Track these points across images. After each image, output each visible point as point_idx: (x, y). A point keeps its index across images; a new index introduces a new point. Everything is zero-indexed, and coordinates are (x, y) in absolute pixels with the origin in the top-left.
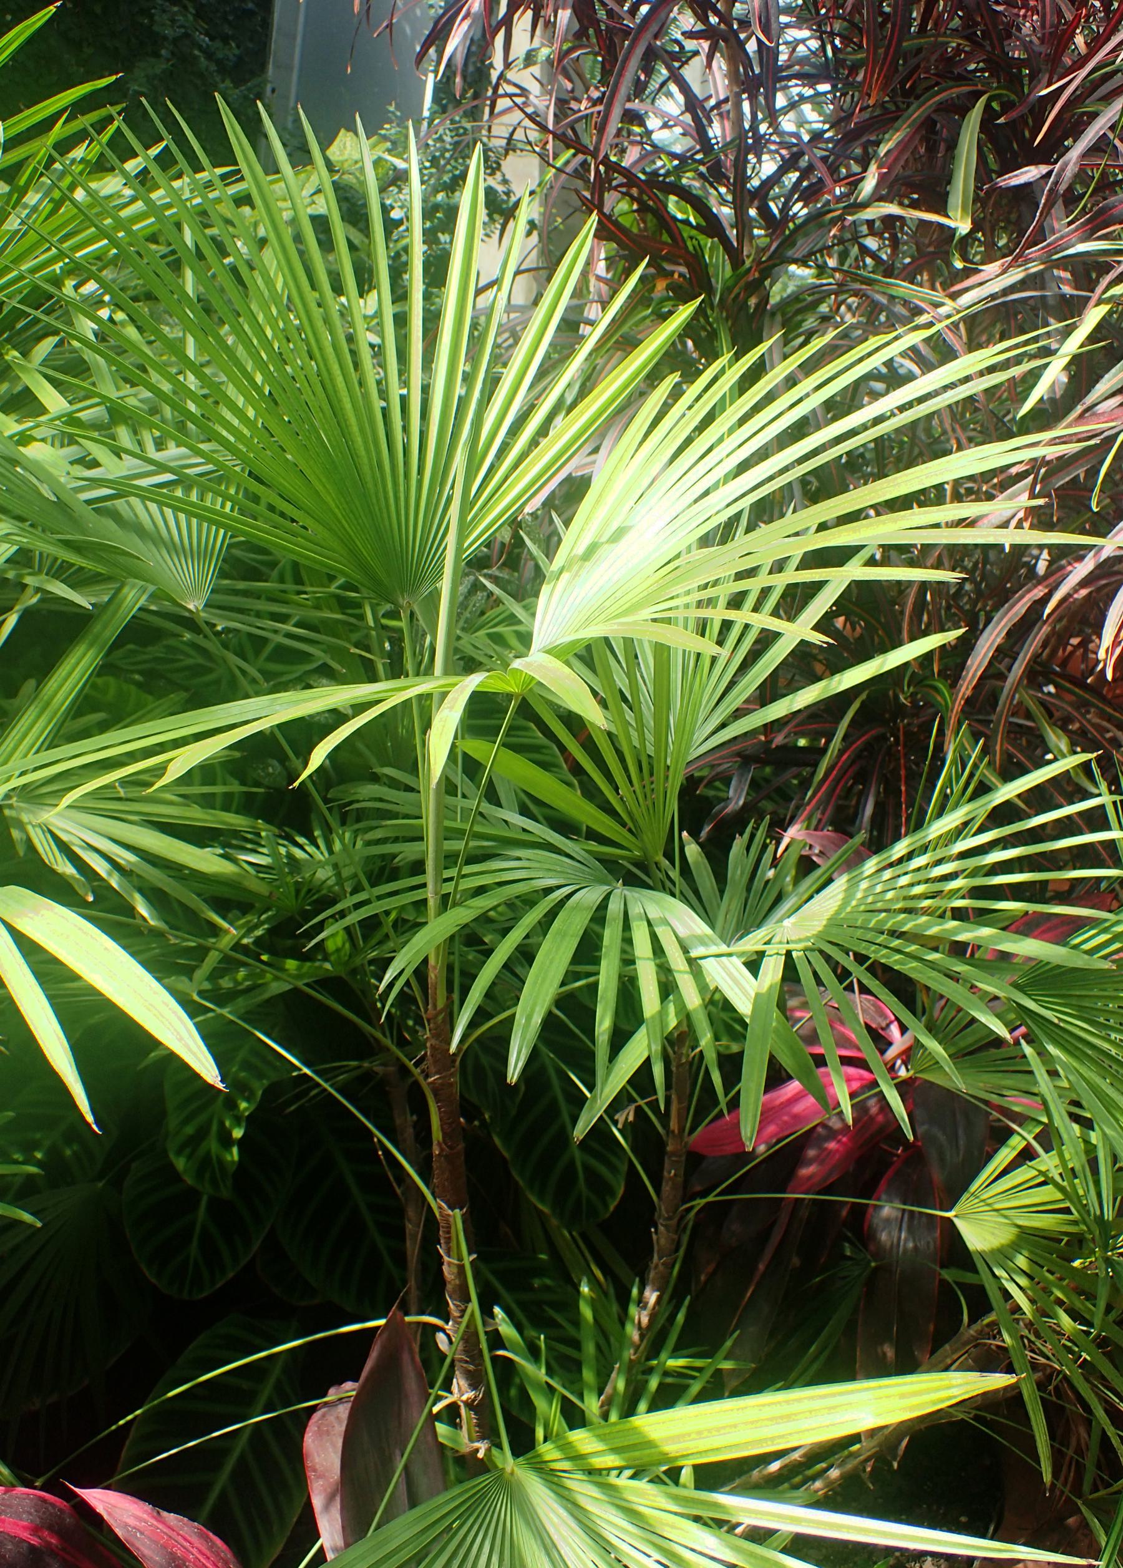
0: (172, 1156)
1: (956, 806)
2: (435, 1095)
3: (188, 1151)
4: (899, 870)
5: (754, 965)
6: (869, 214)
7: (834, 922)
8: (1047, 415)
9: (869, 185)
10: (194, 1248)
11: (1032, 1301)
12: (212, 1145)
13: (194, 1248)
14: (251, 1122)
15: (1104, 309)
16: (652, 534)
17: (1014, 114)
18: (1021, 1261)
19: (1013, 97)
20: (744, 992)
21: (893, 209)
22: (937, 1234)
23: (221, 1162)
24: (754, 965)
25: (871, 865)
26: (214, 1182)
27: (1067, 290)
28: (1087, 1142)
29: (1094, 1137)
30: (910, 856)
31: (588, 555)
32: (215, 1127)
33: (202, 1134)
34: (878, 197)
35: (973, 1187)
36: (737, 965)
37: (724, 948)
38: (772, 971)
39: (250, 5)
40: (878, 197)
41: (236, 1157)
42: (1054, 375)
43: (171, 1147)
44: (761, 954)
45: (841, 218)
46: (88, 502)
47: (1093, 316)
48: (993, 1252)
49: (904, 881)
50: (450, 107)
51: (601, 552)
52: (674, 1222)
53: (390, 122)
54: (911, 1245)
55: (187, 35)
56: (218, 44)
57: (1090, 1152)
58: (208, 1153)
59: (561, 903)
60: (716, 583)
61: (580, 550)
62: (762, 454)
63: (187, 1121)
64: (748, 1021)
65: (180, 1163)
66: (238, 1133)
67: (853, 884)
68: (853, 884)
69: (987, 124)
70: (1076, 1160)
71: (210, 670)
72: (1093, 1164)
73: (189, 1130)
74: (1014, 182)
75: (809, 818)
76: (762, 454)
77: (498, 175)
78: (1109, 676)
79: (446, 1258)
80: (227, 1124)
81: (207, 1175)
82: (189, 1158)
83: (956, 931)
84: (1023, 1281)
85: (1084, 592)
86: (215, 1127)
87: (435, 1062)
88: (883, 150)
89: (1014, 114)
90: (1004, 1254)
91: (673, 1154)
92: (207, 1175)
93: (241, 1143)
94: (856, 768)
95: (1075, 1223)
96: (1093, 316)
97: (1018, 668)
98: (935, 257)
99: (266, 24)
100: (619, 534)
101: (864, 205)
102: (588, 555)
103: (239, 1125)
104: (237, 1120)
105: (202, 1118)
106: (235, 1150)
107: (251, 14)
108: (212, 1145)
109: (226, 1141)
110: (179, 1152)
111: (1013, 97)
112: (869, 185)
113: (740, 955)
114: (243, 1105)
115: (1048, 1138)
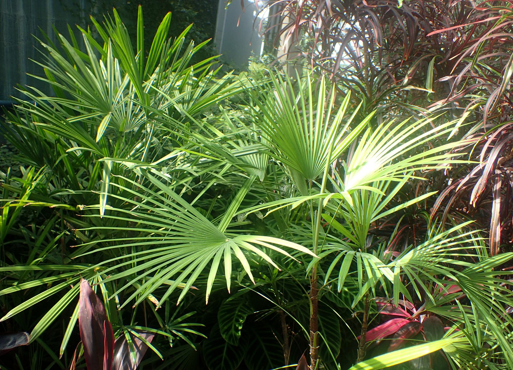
0: (222, 334)
1: (441, 233)
2: (312, 302)
3: (226, 333)
4: (426, 248)
5: (392, 268)
6: (407, 88)
7: (411, 260)
8: (456, 139)
9: (406, 80)
10: (222, 364)
11: (461, 365)
12: (233, 331)
13: (222, 364)
14: (244, 325)
15: (468, 113)
16: (372, 165)
17: (442, 62)
18: (458, 356)
19: (441, 57)
20: (391, 277)
21: (412, 87)
22: (430, 363)
23: (236, 336)
24: (392, 268)
25: (419, 247)
26: (233, 342)
27: (458, 107)
28: (473, 327)
29: (475, 326)
30: (429, 245)
31: (357, 168)
32: (233, 327)
33: (229, 328)
34: (409, 84)
35: (444, 337)
36: (388, 269)
37: (384, 265)
38: (397, 271)
39: (209, 22)
40: (409, 84)
41: (240, 334)
42: (455, 131)
43: (221, 332)
44: (394, 267)
45: (399, 89)
46: (236, 157)
47: (466, 115)
48: (450, 353)
49: (428, 250)
50: (268, 52)
51: (359, 168)
52: (363, 348)
53: (251, 56)
54: (422, 367)
55: (194, 32)
56: (202, 34)
57: (474, 329)
58: (232, 333)
59: (343, 256)
60: (392, 173)
61: (355, 167)
62: (399, 145)
63: (224, 326)
64: (393, 282)
65: (224, 336)
66: (240, 328)
67: (415, 252)
68: (415, 252)
69: (435, 65)
70: (471, 331)
71: (222, 207)
72: (475, 333)
73: (226, 328)
74: (443, 80)
75: (390, 249)
76: (399, 145)
77: (282, 71)
78: (474, 206)
79: (311, 347)
80: (237, 326)
81: (232, 340)
82: (226, 335)
83: (443, 260)
84: (459, 361)
85: (464, 188)
86: (233, 327)
87: (313, 293)
88: (409, 72)
89: (442, 62)
90: (454, 354)
91: (364, 328)
92: (232, 340)
93: (241, 330)
94: (401, 237)
95: (471, 348)
96: (466, 115)
97: (447, 208)
98: (421, 99)
99: (214, 28)
100: (364, 164)
101: (405, 86)
102: (357, 168)
103: (240, 326)
104: (240, 325)
105: (229, 324)
106: (240, 332)
107: (209, 24)
108: (233, 331)
109: (237, 330)
110: (223, 334)
111: (441, 57)
112: (406, 80)
113: (389, 267)
114: (241, 321)
115: (463, 326)
